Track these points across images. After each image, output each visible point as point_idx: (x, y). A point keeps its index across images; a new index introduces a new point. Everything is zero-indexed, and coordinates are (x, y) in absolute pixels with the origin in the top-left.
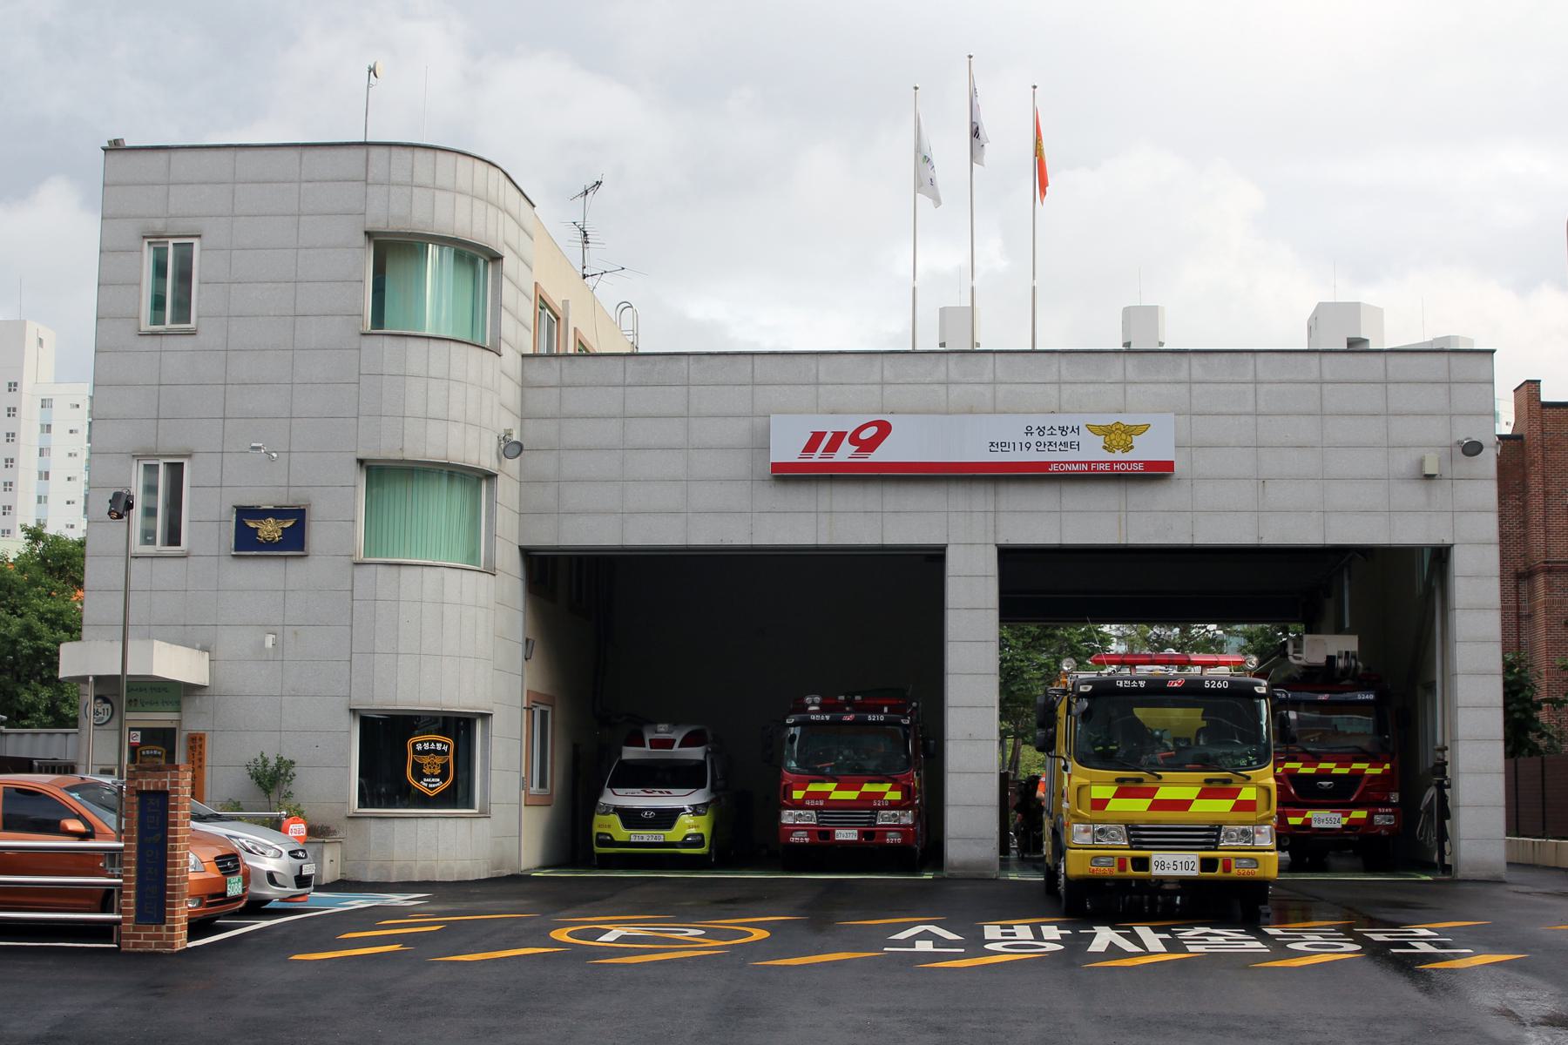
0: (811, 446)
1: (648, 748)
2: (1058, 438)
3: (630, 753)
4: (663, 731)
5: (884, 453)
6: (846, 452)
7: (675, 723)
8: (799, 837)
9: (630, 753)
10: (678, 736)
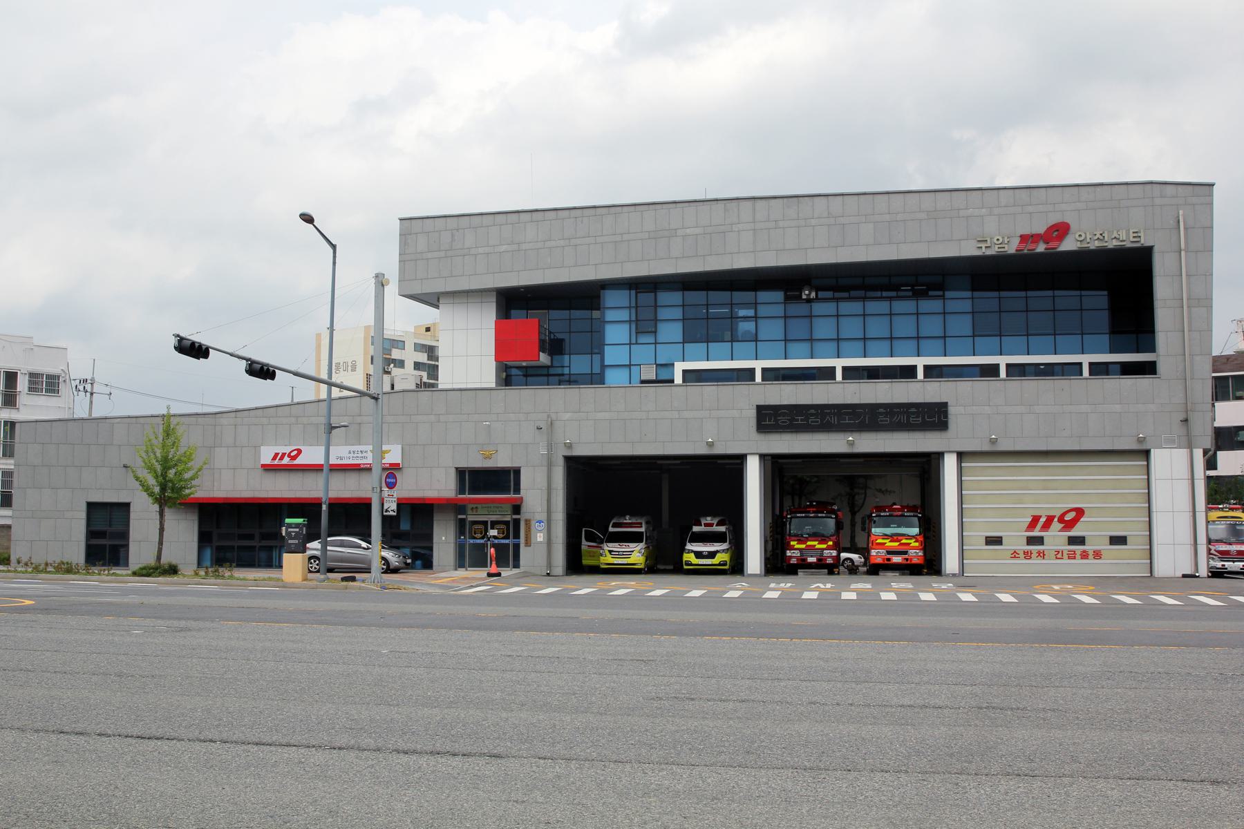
0: (274, 458)
3: (696, 529)
5: (300, 461)
6: (286, 461)
7: (714, 515)
8: (793, 561)
9: (696, 529)
10: (715, 522)
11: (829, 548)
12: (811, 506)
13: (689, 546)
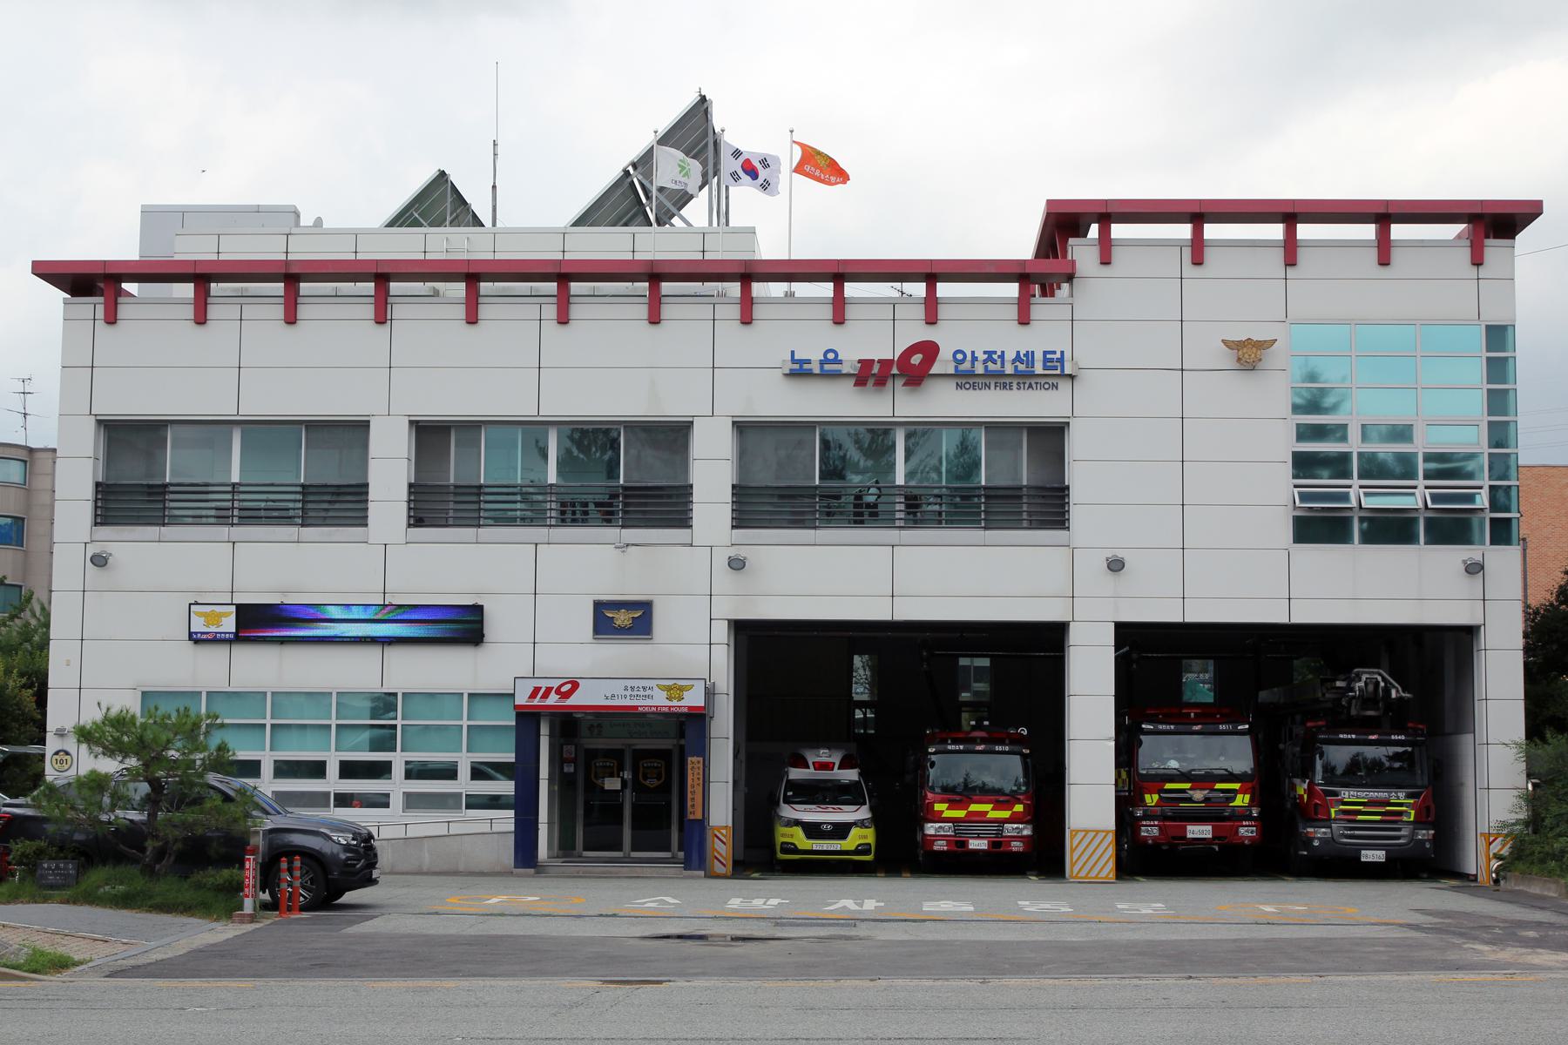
1: (812, 769)
2: (642, 693)
3: (796, 774)
4: (823, 755)
8: (940, 846)
9: (796, 774)
10: (836, 758)
11: (1014, 819)
12: (979, 727)
13: (787, 812)
